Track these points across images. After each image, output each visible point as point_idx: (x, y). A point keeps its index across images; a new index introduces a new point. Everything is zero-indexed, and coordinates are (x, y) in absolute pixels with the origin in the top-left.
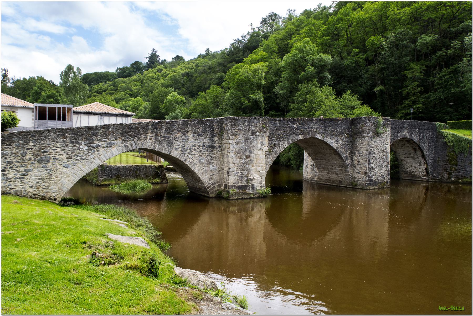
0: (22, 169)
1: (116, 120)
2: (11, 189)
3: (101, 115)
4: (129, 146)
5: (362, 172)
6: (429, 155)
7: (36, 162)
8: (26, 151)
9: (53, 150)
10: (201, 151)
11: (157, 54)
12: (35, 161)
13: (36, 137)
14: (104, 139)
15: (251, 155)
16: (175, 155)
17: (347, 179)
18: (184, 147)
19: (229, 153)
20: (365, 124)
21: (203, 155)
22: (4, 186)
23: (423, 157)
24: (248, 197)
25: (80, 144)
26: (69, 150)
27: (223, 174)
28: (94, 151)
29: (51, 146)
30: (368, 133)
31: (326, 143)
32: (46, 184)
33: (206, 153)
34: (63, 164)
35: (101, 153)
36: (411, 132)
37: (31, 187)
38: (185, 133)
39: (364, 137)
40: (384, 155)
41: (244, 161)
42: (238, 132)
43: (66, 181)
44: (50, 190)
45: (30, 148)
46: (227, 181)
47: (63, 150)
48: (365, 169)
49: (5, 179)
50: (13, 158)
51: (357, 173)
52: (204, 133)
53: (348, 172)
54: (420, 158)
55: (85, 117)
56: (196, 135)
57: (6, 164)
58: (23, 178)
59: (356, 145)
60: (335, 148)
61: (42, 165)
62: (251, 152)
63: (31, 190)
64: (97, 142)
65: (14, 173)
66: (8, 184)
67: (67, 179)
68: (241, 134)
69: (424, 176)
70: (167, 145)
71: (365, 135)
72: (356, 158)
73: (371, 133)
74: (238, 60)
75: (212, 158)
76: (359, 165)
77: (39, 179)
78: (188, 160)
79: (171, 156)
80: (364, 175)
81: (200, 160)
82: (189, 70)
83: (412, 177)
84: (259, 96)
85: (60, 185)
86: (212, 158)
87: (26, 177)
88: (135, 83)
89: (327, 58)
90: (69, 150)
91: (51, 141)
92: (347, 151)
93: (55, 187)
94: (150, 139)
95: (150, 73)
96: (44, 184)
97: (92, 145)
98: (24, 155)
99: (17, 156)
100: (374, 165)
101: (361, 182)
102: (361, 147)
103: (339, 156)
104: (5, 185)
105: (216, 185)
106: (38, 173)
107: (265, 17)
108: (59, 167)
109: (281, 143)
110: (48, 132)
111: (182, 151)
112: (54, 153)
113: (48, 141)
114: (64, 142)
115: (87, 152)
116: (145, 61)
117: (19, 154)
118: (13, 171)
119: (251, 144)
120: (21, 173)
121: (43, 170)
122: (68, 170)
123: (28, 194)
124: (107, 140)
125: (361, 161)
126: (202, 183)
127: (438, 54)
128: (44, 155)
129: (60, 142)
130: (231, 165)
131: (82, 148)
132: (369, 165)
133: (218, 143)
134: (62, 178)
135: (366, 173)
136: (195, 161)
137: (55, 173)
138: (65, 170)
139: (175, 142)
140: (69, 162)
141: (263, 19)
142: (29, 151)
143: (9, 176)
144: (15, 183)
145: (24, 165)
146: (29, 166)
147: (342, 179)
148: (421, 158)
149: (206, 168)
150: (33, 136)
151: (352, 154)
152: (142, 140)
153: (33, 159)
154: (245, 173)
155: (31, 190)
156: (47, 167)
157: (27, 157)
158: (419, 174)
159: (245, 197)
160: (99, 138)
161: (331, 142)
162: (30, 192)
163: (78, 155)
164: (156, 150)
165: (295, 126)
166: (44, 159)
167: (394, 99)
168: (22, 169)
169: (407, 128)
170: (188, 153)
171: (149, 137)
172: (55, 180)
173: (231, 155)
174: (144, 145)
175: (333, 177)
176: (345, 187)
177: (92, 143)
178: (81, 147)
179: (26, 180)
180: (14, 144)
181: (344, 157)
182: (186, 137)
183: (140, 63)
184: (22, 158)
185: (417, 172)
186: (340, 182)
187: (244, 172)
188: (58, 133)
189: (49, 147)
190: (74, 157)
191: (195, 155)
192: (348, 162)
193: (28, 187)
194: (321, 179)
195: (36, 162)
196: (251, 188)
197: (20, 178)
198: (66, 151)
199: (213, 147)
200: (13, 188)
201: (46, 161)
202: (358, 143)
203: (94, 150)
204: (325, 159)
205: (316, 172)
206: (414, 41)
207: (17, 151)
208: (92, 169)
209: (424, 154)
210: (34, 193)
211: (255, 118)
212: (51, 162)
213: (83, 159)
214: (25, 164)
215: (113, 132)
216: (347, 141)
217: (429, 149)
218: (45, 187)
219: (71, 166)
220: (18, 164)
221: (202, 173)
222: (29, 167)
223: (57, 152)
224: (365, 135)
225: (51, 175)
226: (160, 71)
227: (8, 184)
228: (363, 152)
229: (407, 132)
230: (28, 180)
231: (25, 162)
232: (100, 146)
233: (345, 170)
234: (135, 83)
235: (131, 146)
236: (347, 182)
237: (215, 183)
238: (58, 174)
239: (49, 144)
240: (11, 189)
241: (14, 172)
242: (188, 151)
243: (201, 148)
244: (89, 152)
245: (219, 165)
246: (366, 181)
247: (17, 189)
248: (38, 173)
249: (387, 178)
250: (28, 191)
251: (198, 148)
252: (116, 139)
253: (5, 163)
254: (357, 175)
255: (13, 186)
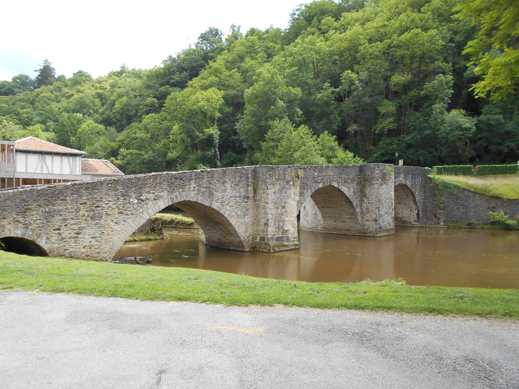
0: (76, 227)
1: (61, 161)
2: (65, 250)
3: (43, 154)
4: (174, 198)
5: (372, 220)
6: (420, 200)
7: (89, 219)
8: (80, 206)
9: (105, 204)
10: (237, 202)
11: (52, 66)
12: (88, 217)
13: (89, 190)
14: (152, 191)
15: (287, 205)
16: (215, 208)
17: (357, 227)
18: (223, 198)
19: (267, 203)
20: (374, 171)
21: (240, 206)
22: (59, 247)
23: (415, 202)
24: (285, 249)
25: (130, 197)
26: (121, 204)
27: (259, 225)
28: (143, 205)
29: (103, 200)
30: (378, 180)
31: (340, 191)
32: (98, 243)
33: (242, 204)
34: (115, 221)
35: (149, 207)
36: (405, 178)
37: (84, 247)
38: (224, 183)
39: (373, 184)
40: (390, 202)
41: (280, 212)
42: (276, 182)
43: (116, 239)
44: (102, 249)
45: (84, 203)
46: (265, 233)
47: (115, 204)
48: (375, 216)
49: (60, 239)
50: (68, 214)
51: (366, 220)
52: (240, 182)
53: (358, 220)
54: (411, 203)
55: (33, 159)
56: (233, 185)
57: (61, 222)
58: (77, 237)
59: (365, 192)
60: (348, 196)
61: (95, 222)
62: (285, 203)
63: (84, 250)
64: (146, 194)
65: (69, 232)
66: (63, 244)
67: (118, 237)
68: (277, 184)
69: (415, 222)
70: (208, 196)
71: (375, 182)
72: (365, 206)
73: (380, 180)
74: (173, 83)
75: (247, 209)
76: (368, 212)
77: (92, 238)
78: (227, 212)
79: (212, 208)
80: (374, 223)
81: (237, 211)
82: (100, 91)
83: (403, 223)
84: (214, 131)
85: (111, 244)
86: (247, 209)
87: (80, 236)
88: (23, 104)
89: (297, 91)
90: (121, 204)
91: (104, 194)
92: (357, 198)
93: (106, 246)
94: (193, 190)
95: (45, 91)
96: (96, 243)
97: (141, 197)
98: (78, 210)
99: (72, 212)
100: (382, 212)
101: (371, 229)
102: (371, 195)
103: (350, 203)
104: (59, 246)
105: (250, 238)
106: (92, 231)
107: (203, 32)
108: (111, 223)
109: (305, 192)
110: (101, 184)
111: (222, 203)
112: (106, 208)
113: (101, 194)
114: (116, 195)
115: (137, 206)
116: (34, 76)
117: (73, 210)
118: (67, 229)
119: (286, 193)
120: (75, 232)
121: (96, 227)
122: (119, 226)
123: (81, 255)
124: (154, 191)
125: (370, 208)
126: (239, 237)
127: (412, 93)
128: (97, 210)
129: (112, 195)
130: (270, 216)
131: (133, 202)
132: (379, 212)
133: (252, 193)
134: (114, 236)
135: (376, 221)
136: (233, 214)
137: (107, 230)
138: (116, 227)
139: (215, 192)
140: (120, 218)
141: (202, 34)
142: (83, 206)
143: (63, 235)
144: (69, 243)
145: (78, 223)
146: (83, 223)
147: (351, 227)
148: (412, 204)
149: (242, 220)
150: (87, 189)
151: (362, 201)
152: (186, 192)
153: (86, 215)
154: (281, 224)
155: (84, 250)
156: (99, 224)
157: (81, 213)
158: (410, 220)
159: (282, 249)
160: (148, 189)
161: (344, 189)
162: (83, 253)
163: (128, 209)
164: (199, 202)
165: (316, 174)
166: (97, 215)
167: (395, 146)
168: (76, 227)
169: (402, 173)
170: (227, 205)
171: (192, 189)
172: (107, 238)
173: (270, 206)
174: (188, 197)
175: (340, 225)
176: (353, 235)
177: (141, 196)
178: (132, 200)
179: (79, 239)
180: (68, 198)
181: (355, 204)
182: (224, 187)
183: (27, 77)
184: (76, 214)
185: (408, 218)
186: (349, 230)
187: (280, 223)
188: (109, 185)
189: (101, 201)
190: (125, 212)
191: (232, 206)
192: (358, 210)
193: (82, 247)
194: (326, 228)
195: (89, 219)
196: (286, 240)
197: (74, 238)
198: (117, 205)
199: (248, 198)
200: (67, 249)
201: (99, 217)
202: (367, 191)
203: (143, 203)
204: (333, 207)
205: (319, 221)
206: (386, 79)
207: (71, 206)
208: (141, 225)
209: (415, 200)
210: (86, 254)
211: (289, 167)
212: (103, 218)
213: (132, 214)
214: (79, 221)
215: (160, 183)
216: (357, 189)
217: (420, 194)
218: (97, 247)
219: (121, 221)
220: (72, 222)
221: (239, 226)
222: (83, 225)
223: (110, 207)
224: (375, 182)
225: (103, 233)
226: (59, 89)
227: (63, 244)
228: (372, 199)
229: (403, 178)
230: (82, 239)
231: (79, 219)
232: (148, 199)
233: (355, 218)
234: (23, 104)
235: (177, 198)
236: (356, 231)
237: (249, 236)
238: (110, 231)
239: (102, 198)
240: (65, 250)
241: (68, 230)
242: (226, 202)
243: (238, 198)
244: (139, 206)
245: (253, 217)
246: (377, 229)
247: (71, 249)
248: (92, 231)
249: (392, 225)
250: (82, 251)
251: (235, 199)
252: (163, 191)
253: (60, 220)
254: (366, 223)
255: (67, 247)
